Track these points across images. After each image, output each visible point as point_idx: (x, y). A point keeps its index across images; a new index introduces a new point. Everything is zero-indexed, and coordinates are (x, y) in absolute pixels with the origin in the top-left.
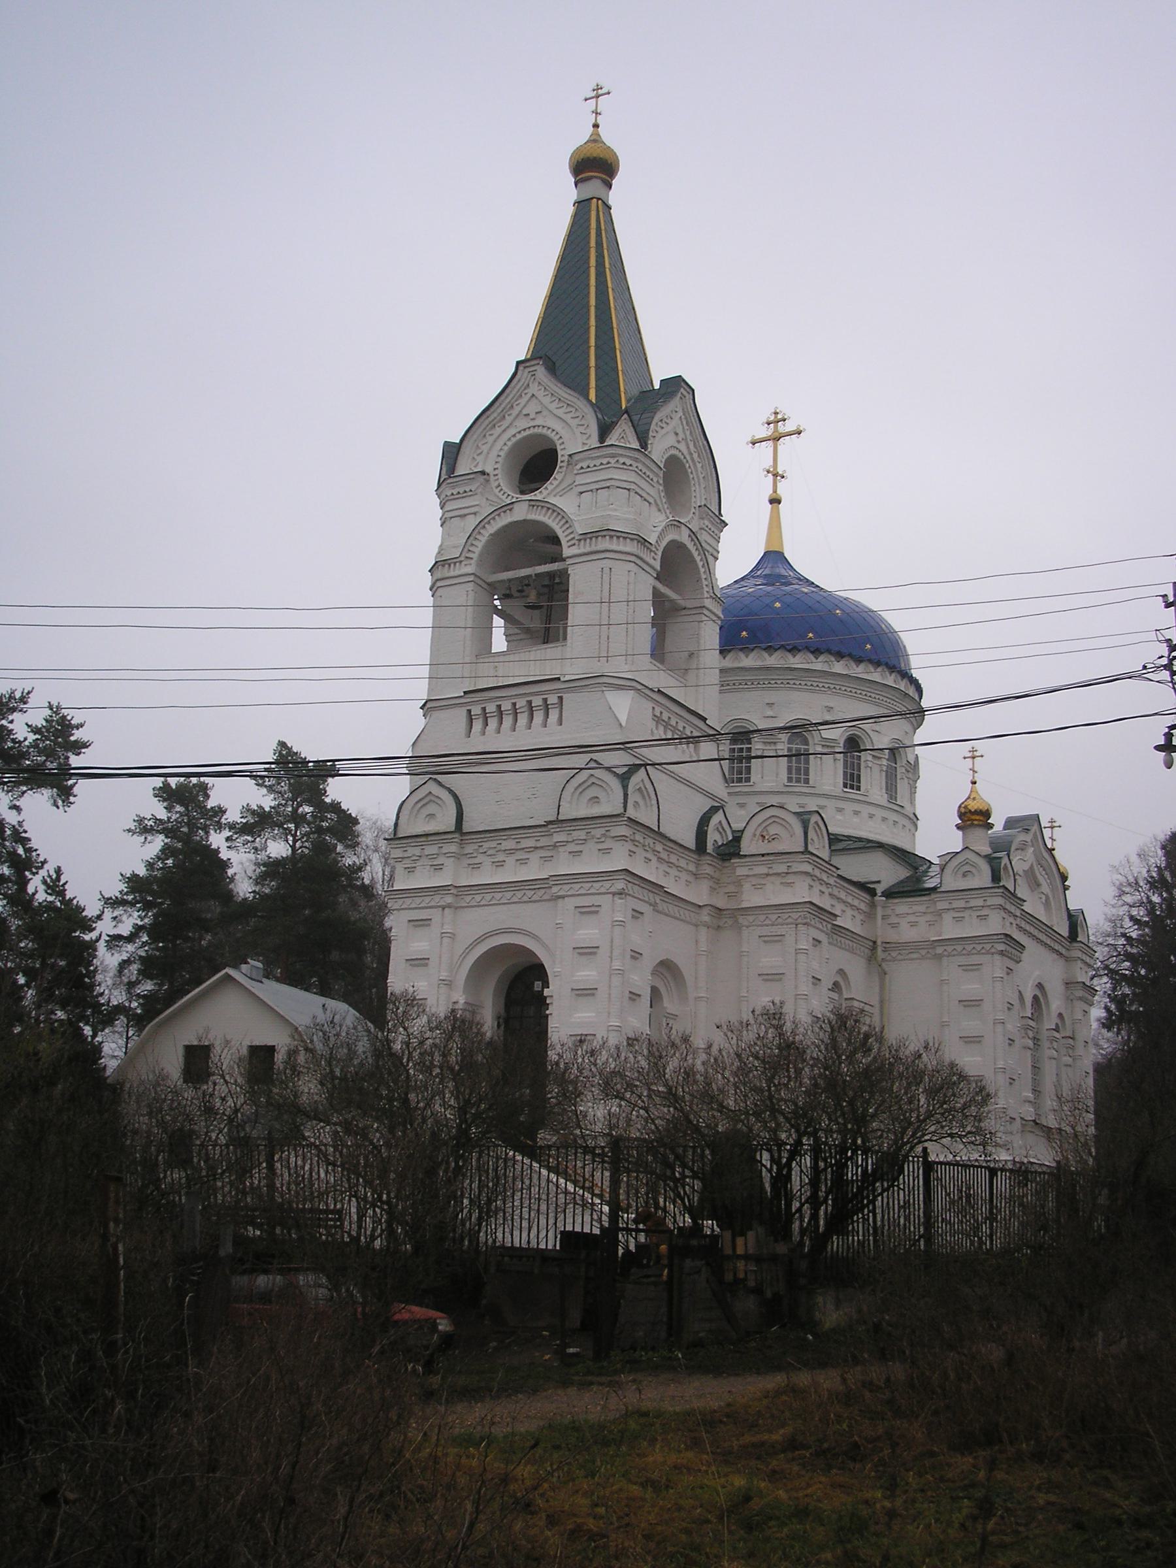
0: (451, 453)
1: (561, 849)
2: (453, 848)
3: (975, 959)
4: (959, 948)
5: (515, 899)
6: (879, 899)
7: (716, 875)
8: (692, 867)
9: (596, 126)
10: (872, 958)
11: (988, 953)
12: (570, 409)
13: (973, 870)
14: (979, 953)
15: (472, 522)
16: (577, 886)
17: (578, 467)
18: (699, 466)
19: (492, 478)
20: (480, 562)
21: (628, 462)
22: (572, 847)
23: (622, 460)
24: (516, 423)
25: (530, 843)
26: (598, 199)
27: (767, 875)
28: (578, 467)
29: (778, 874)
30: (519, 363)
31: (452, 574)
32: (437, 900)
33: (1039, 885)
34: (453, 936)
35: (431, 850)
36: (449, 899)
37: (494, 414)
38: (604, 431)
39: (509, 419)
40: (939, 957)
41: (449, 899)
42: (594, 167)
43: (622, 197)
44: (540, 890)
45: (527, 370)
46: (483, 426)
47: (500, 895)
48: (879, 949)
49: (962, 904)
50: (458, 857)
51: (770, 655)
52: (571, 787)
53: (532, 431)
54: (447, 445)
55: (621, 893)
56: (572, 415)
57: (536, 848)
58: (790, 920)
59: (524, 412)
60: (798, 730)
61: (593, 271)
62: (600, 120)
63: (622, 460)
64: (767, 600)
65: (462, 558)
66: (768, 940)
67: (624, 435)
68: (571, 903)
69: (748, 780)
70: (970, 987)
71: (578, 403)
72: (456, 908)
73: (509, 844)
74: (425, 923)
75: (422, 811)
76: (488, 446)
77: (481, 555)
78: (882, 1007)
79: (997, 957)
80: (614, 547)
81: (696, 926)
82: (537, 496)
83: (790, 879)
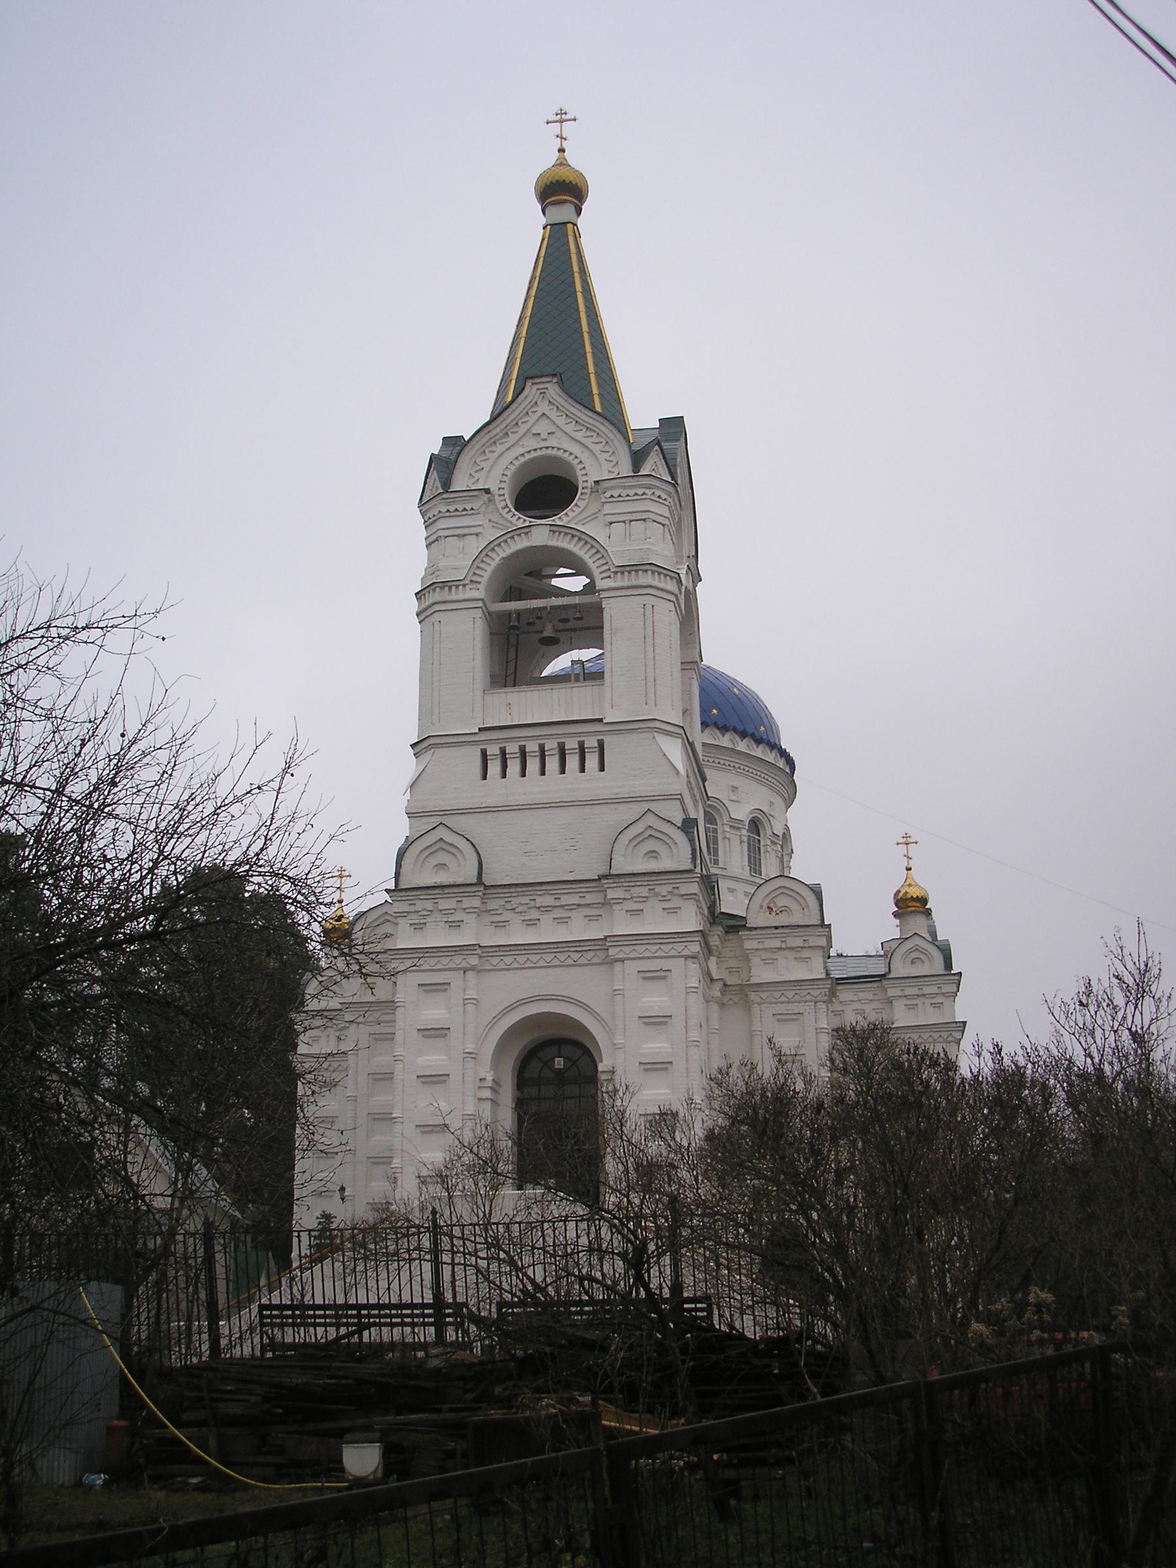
0: (445, 463)
1: (615, 907)
2: (476, 902)
5: (556, 962)
9: (562, 150)
13: (922, 956)
15: (474, 546)
17: (608, 495)
21: (664, 496)
23: (658, 493)
25: (575, 900)
27: (780, 949)
28: (608, 495)
29: (791, 949)
31: (454, 597)
32: (458, 961)
35: (444, 904)
36: (474, 961)
39: (513, 438)
41: (474, 961)
42: (561, 191)
44: (603, 951)
46: (484, 440)
47: (538, 957)
49: (915, 991)
53: (544, 452)
57: (579, 905)
58: (808, 997)
61: (580, 296)
62: (565, 144)
63: (658, 493)
65: (467, 582)
68: (633, 967)
71: (601, 427)
72: (479, 971)
73: (548, 900)
74: (443, 987)
75: (640, 846)
76: (489, 463)
80: (662, 585)
82: (555, 520)
83: (805, 953)
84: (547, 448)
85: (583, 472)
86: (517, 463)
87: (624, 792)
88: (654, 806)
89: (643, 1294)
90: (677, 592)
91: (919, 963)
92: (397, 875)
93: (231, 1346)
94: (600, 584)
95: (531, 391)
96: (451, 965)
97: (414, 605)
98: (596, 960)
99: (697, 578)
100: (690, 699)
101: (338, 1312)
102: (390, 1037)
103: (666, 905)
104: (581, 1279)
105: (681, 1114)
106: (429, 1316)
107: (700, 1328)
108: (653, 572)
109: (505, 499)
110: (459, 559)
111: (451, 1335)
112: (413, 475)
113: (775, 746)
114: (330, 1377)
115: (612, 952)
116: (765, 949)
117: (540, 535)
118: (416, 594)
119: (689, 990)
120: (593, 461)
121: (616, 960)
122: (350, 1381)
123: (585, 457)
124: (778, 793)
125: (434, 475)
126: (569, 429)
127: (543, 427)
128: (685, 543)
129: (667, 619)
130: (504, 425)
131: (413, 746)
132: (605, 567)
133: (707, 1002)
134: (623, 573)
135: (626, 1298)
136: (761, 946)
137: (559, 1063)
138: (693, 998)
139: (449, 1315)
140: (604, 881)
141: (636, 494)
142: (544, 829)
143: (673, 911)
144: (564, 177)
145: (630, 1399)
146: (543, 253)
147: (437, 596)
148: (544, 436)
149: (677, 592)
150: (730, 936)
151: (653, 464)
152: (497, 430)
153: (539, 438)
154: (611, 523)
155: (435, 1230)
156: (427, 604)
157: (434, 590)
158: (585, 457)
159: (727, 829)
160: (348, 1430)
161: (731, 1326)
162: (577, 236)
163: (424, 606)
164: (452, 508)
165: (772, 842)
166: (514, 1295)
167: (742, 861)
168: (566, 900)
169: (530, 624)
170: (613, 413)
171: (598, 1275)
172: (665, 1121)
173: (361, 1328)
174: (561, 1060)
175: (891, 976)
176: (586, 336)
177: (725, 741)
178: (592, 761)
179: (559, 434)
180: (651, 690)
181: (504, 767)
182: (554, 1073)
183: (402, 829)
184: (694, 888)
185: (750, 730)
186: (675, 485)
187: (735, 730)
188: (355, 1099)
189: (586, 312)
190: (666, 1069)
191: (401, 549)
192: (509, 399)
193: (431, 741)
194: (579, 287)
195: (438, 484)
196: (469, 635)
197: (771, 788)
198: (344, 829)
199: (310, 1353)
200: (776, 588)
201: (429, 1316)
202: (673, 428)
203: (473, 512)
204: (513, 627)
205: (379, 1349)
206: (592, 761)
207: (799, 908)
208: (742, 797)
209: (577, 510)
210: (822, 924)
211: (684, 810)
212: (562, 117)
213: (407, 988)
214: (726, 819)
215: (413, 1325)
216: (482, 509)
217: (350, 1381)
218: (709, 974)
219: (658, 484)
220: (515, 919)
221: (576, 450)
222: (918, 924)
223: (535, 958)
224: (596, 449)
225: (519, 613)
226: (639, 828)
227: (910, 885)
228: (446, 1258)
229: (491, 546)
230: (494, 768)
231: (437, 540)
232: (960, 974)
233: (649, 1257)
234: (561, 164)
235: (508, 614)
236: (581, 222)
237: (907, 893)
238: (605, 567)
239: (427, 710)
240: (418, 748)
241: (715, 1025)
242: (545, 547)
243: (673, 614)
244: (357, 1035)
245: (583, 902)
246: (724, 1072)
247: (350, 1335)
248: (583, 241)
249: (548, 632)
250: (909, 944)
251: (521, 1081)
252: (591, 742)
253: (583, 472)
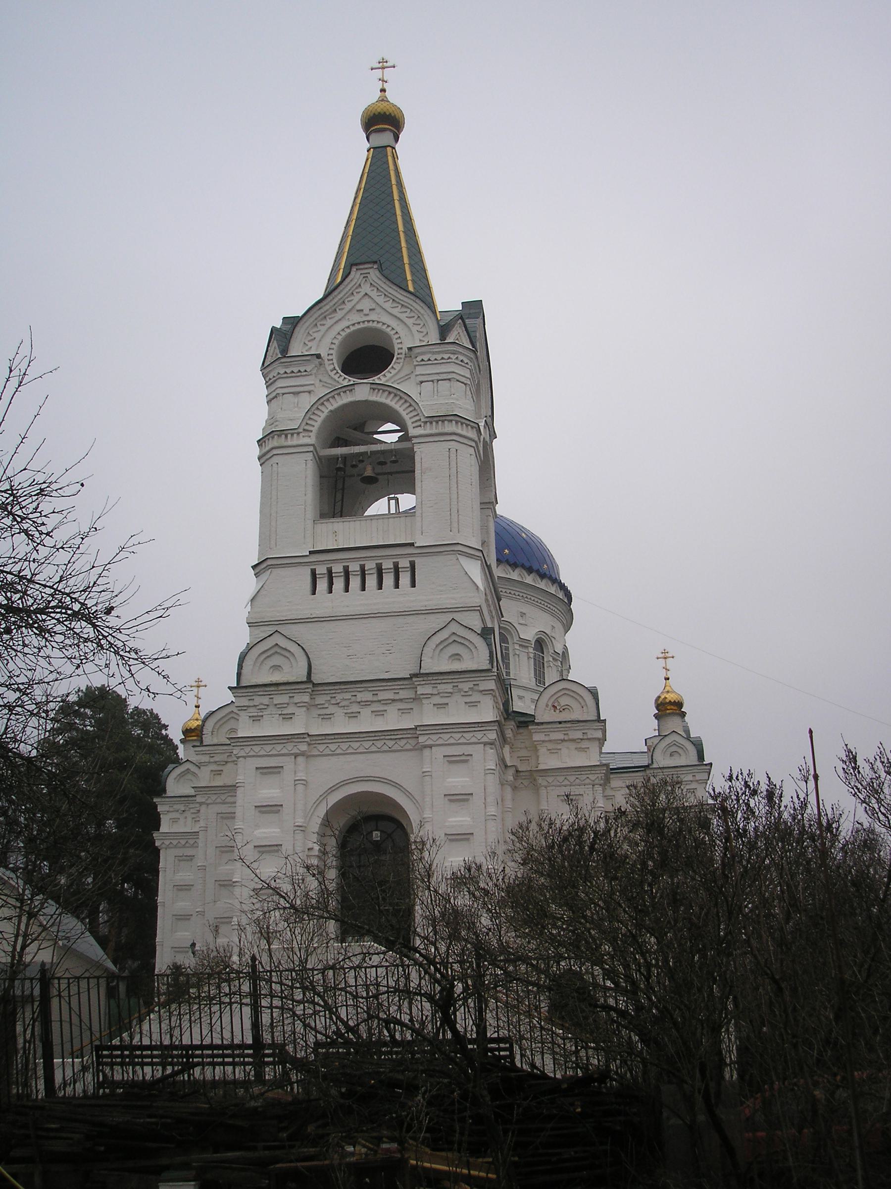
0: (282, 336)
1: (424, 701)
2: (306, 698)
5: (374, 749)
9: (383, 90)
15: (307, 401)
16: (446, 736)
17: (419, 359)
21: (466, 361)
22: (437, 700)
23: (461, 358)
24: (349, 316)
25: (389, 695)
28: (419, 359)
31: (289, 443)
32: (290, 747)
34: (305, 783)
35: (278, 699)
36: (304, 747)
39: (339, 314)
41: (304, 747)
42: (383, 122)
43: (409, 153)
44: (413, 739)
45: (359, 272)
46: (316, 315)
47: (358, 744)
50: (309, 707)
52: (432, 644)
57: (393, 700)
58: (588, 781)
59: (358, 307)
62: (386, 86)
63: (461, 358)
68: (439, 752)
71: (414, 304)
72: (308, 757)
73: (367, 696)
74: (277, 770)
75: (445, 650)
76: (321, 334)
83: (585, 744)
84: (368, 321)
85: (399, 341)
86: (343, 334)
87: (432, 604)
88: (457, 616)
89: (449, 1035)
90: (476, 439)
91: (676, 756)
92: (239, 675)
93: (65, 1084)
94: (412, 432)
95: (355, 275)
96: (284, 751)
97: (256, 451)
98: (408, 747)
99: (493, 435)
100: (488, 533)
101: (165, 1052)
102: (232, 816)
103: (468, 699)
104: (387, 1022)
105: (484, 868)
106: (248, 1056)
107: (504, 1068)
108: (457, 422)
109: (333, 363)
110: (294, 412)
111: (269, 1074)
112: (258, 345)
113: (556, 581)
114: (150, 1116)
115: (421, 739)
116: (550, 741)
117: (363, 392)
118: (258, 441)
119: (488, 772)
120: (406, 332)
121: (426, 747)
122: (169, 1121)
123: (399, 328)
124: (559, 619)
125: (275, 344)
126: (388, 305)
127: (366, 305)
128: (483, 404)
129: (468, 461)
130: (333, 302)
131: (254, 567)
132: (417, 418)
133: (502, 785)
134: (431, 423)
135: (433, 1042)
136: (547, 739)
137: (376, 835)
138: (490, 778)
139: (268, 1056)
140: (414, 679)
141: (443, 358)
142: (363, 636)
143: (473, 704)
144: (385, 110)
145: (439, 1141)
146: (367, 170)
147: (275, 442)
148: (366, 311)
149: (476, 439)
150: (521, 730)
151: (457, 334)
152: (327, 307)
153: (361, 314)
154: (422, 382)
155: (254, 976)
156: (267, 449)
157: (273, 438)
158: (399, 328)
159: (517, 647)
160: (167, 1168)
161: (533, 1065)
162: (395, 158)
163: (264, 450)
164: (288, 371)
165: (554, 659)
166: (327, 1037)
167: (529, 668)
168: (383, 696)
169: (354, 466)
170: (423, 295)
171: (406, 1018)
172: (466, 879)
173: (190, 1066)
174: (379, 833)
175: (655, 766)
176: (402, 235)
177: (515, 575)
178: (405, 579)
179: (378, 310)
180: (455, 518)
181: (331, 584)
182: (371, 847)
183: (243, 637)
184: (491, 685)
185: (535, 567)
186: (475, 352)
187: (523, 566)
188: (203, 868)
189: (402, 216)
190: (468, 839)
191: (245, 406)
192: (339, 280)
193: (269, 562)
194: (396, 197)
195: (278, 351)
196: (301, 474)
197: (552, 615)
198: (134, 540)
199: (139, 1091)
200: (556, 452)
201: (248, 1056)
202: (473, 310)
203: (306, 373)
204: (339, 469)
205: (204, 1085)
206: (405, 579)
207: (579, 706)
208: (529, 621)
209: (393, 372)
210: (599, 720)
211: (483, 621)
212: (383, 65)
213: (244, 772)
214: (516, 639)
215: (234, 1064)
216: (315, 371)
217: (169, 1121)
218: (503, 760)
219: (461, 350)
220: (339, 712)
221: (393, 323)
222: (673, 723)
223: (355, 745)
224: (410, 322)
225: (345, 458)
226: (444, 634)
227: (668, 692)
228: (265, 1002)
229: (321, 402)
230: (322, 585)
231: (276, 397)
232: (711, 764)
233: (456, 1001)
234: (383, 100)
235: (336, 458)
236: (397, 147)
237: (666, 698)
238: (417, 418)
239: (266, 535)
240: (257, 570)
241: (509, 804)
242: (366, 401)
243: (474, 457)
244: (209, 814)
245: (397, 697)
246: (524, 827)
247: (175, 1074)
248: (400, 162)
249: (369, 472)
250: (668, 740)
251: (343, 845)
252: (404, 563)
253: (399, 341)
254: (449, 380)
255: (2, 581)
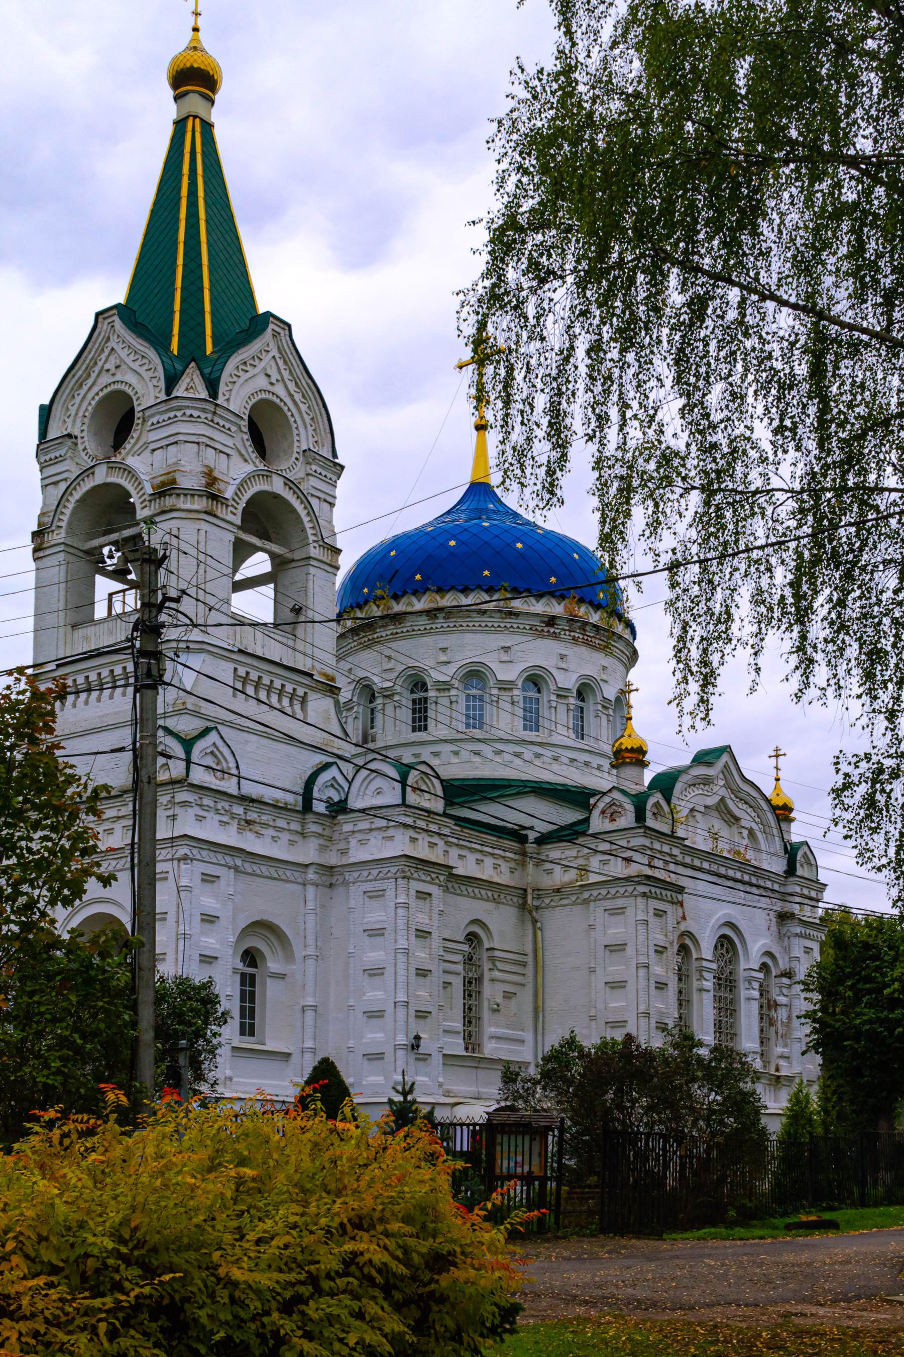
3: (620, 902)
4: (604, 892)
6: (531, 848)
7: (327, 832)
8: (295, 826)
10: (523, 906)
11: (631, 895)
12: (145, 361)
14: (623, 896)
15: (63, 486)
17: (150, 423)
18: (303, 408)
19: (79, 441)
20: (70, 531)
21: (196, 413)
23: (188, 412)
26: (195, 117)
27: (371, 830)
28: (150, 423)
29: (380, 829)
30: (98, 315)
33: (738, 819)
37: (79, 372)
38: (171, 381)
39: (93, 375)
40: (586, 902)
42: (194, 79)
48: (529, 898)
51: (442, 598)
54: (42, 407)
55: (185, 858)
56: (146, 367)
59: (106, 367)
60: (475, 675)
61: (184, 202)
63: (188, 412)
64: (441, 540)
65: (53, 528)
66: (372, 895)
67: (191, 384)
69: (426, 729)
70: (616, 931)
77: (70, 523)
78: (536, 956)
79: (639, 899)
81: (304, 885)
83: (391, 832)
141: (191, 416)
154: (154, 450)
165: (604, 707)
219: (187, 403)
234: (195, 48)
245: (120, 814)
254: (176, 443)
255: (6, 697)
